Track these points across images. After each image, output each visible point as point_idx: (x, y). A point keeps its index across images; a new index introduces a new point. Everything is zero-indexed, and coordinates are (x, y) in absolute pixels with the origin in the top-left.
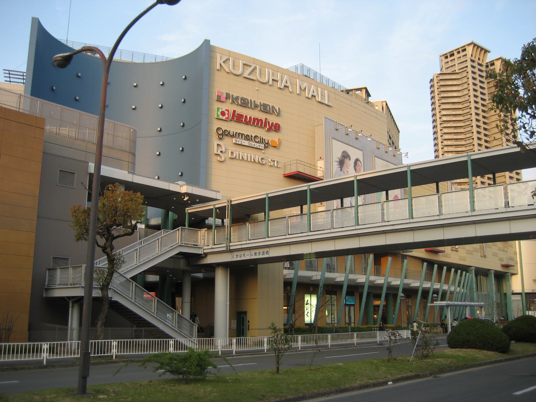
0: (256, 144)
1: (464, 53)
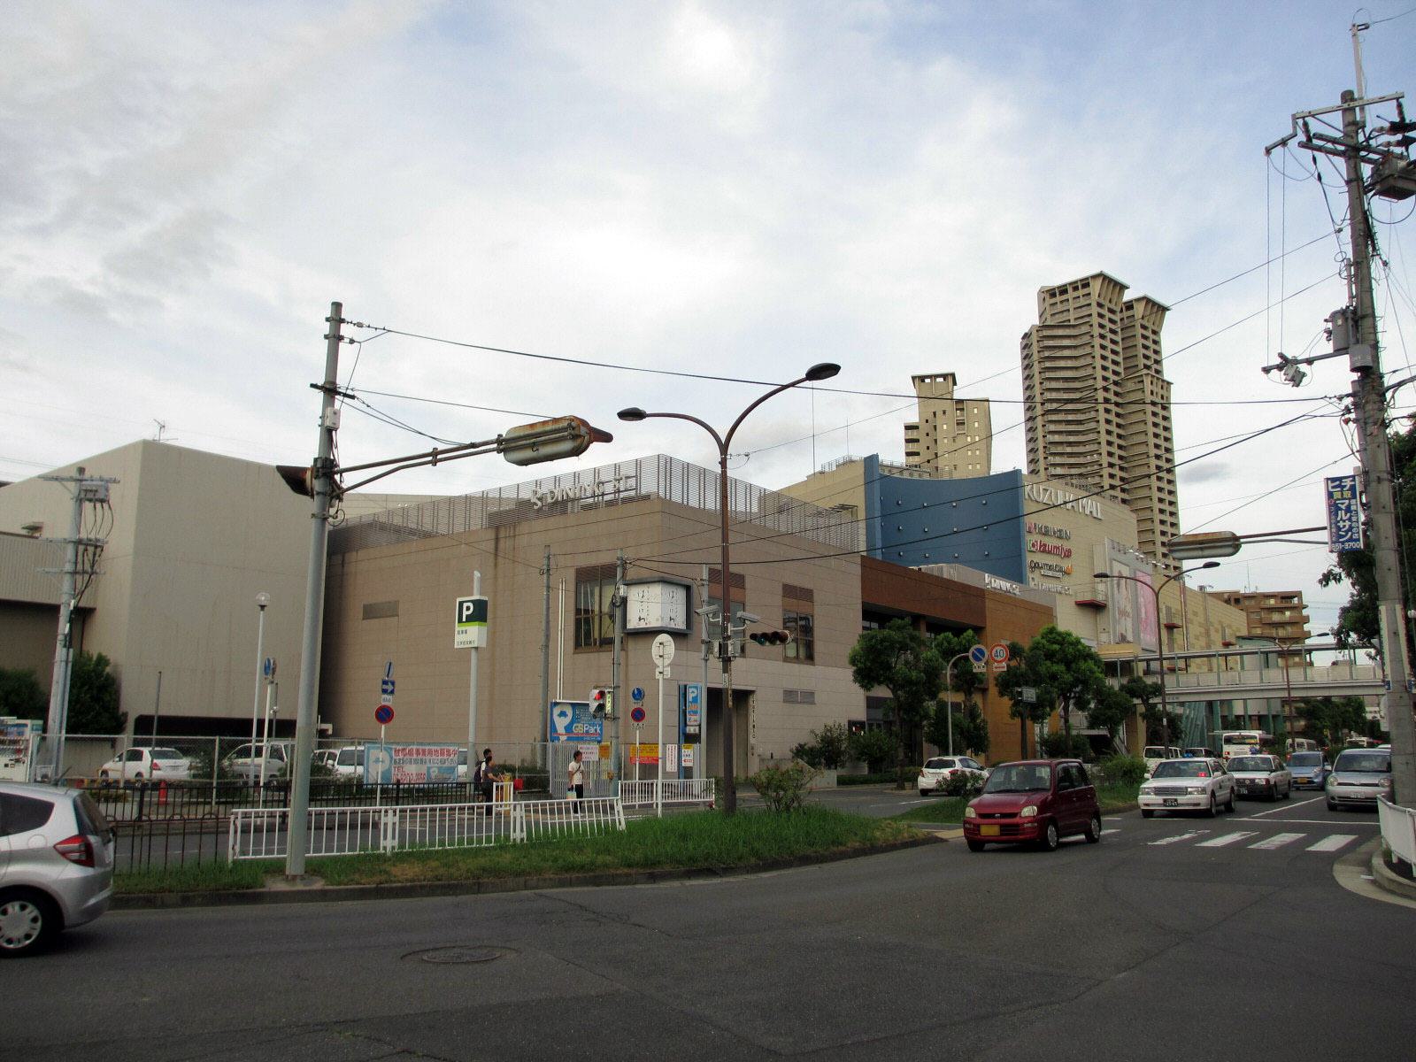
1: (1086, 291)
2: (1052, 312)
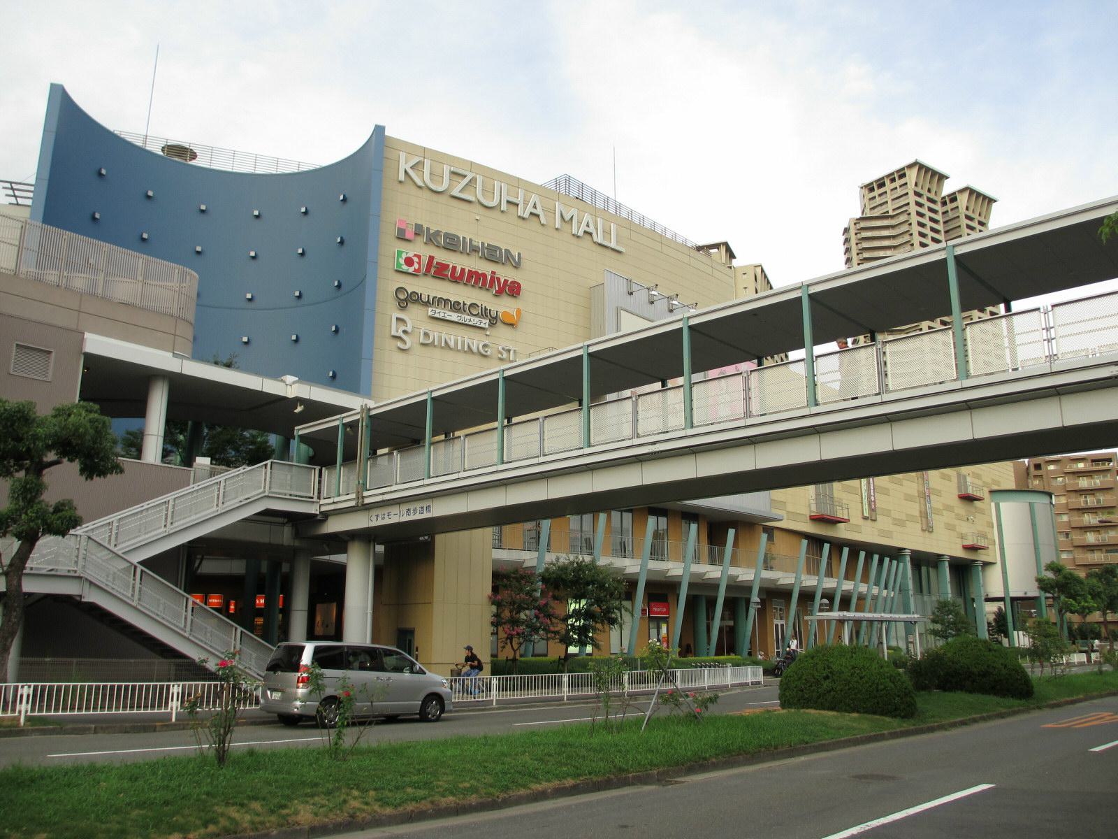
0: (472, 318)
1: (903, 181)
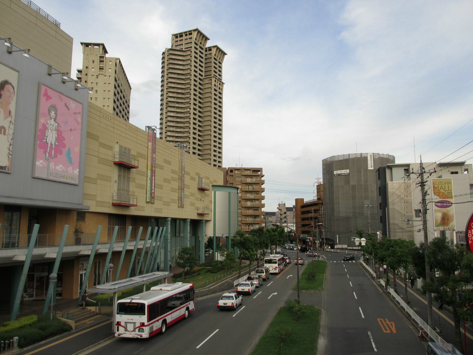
1: (190, 36)
2: (176, 45)
